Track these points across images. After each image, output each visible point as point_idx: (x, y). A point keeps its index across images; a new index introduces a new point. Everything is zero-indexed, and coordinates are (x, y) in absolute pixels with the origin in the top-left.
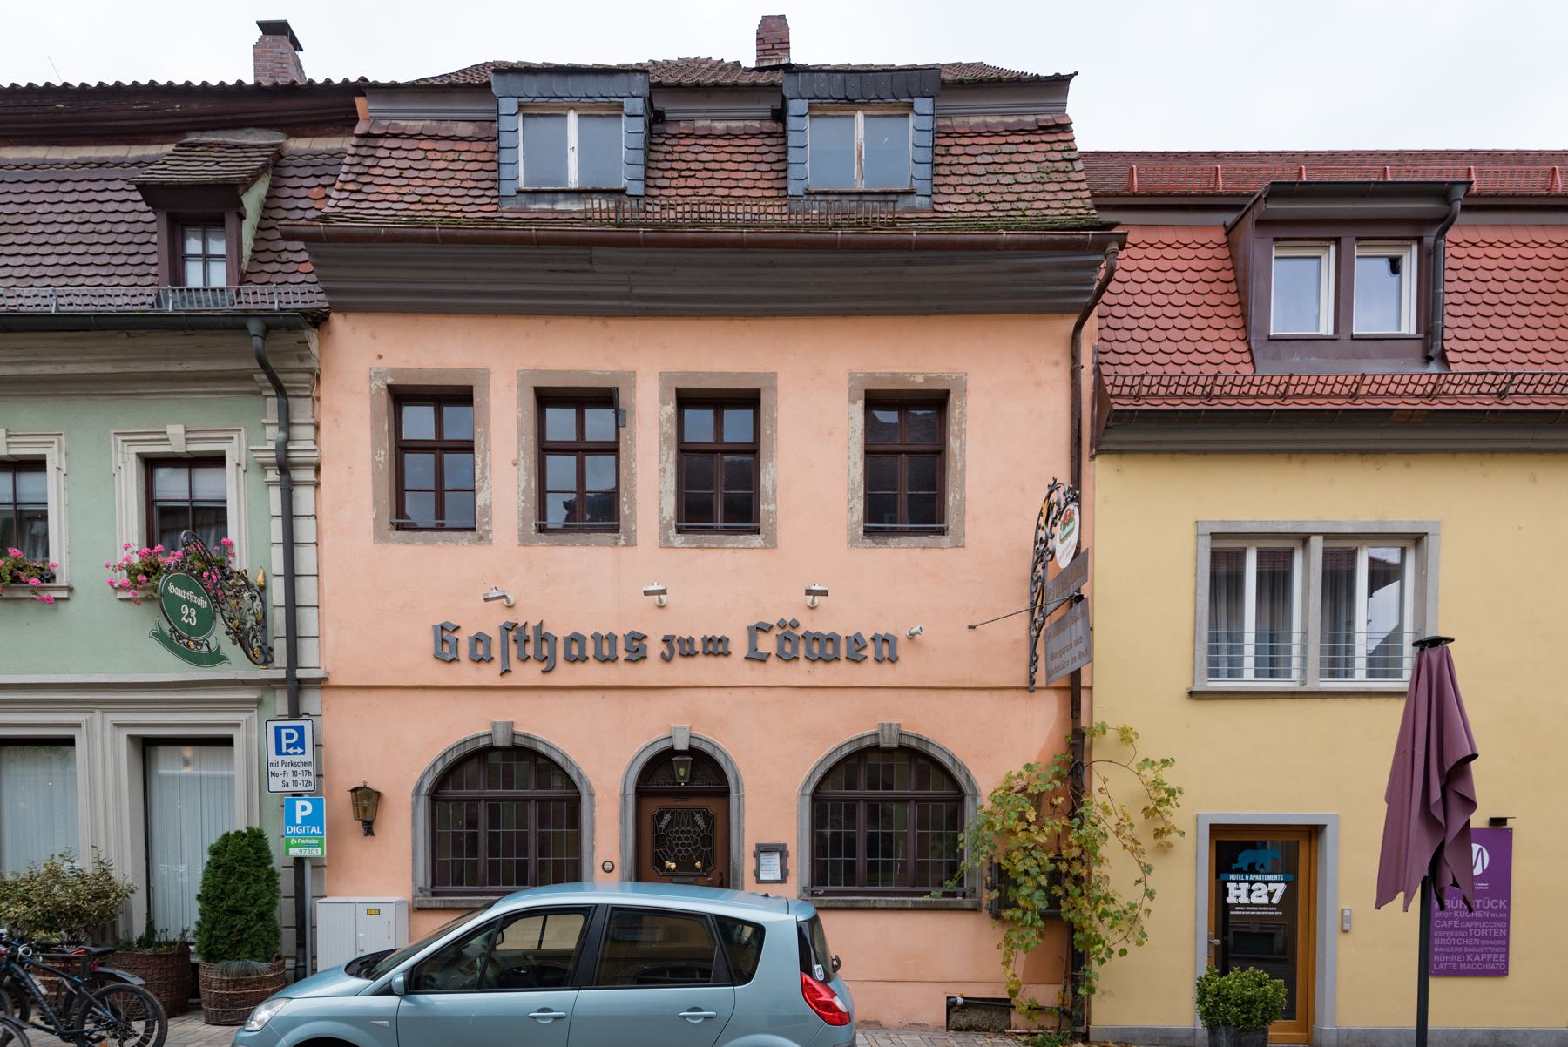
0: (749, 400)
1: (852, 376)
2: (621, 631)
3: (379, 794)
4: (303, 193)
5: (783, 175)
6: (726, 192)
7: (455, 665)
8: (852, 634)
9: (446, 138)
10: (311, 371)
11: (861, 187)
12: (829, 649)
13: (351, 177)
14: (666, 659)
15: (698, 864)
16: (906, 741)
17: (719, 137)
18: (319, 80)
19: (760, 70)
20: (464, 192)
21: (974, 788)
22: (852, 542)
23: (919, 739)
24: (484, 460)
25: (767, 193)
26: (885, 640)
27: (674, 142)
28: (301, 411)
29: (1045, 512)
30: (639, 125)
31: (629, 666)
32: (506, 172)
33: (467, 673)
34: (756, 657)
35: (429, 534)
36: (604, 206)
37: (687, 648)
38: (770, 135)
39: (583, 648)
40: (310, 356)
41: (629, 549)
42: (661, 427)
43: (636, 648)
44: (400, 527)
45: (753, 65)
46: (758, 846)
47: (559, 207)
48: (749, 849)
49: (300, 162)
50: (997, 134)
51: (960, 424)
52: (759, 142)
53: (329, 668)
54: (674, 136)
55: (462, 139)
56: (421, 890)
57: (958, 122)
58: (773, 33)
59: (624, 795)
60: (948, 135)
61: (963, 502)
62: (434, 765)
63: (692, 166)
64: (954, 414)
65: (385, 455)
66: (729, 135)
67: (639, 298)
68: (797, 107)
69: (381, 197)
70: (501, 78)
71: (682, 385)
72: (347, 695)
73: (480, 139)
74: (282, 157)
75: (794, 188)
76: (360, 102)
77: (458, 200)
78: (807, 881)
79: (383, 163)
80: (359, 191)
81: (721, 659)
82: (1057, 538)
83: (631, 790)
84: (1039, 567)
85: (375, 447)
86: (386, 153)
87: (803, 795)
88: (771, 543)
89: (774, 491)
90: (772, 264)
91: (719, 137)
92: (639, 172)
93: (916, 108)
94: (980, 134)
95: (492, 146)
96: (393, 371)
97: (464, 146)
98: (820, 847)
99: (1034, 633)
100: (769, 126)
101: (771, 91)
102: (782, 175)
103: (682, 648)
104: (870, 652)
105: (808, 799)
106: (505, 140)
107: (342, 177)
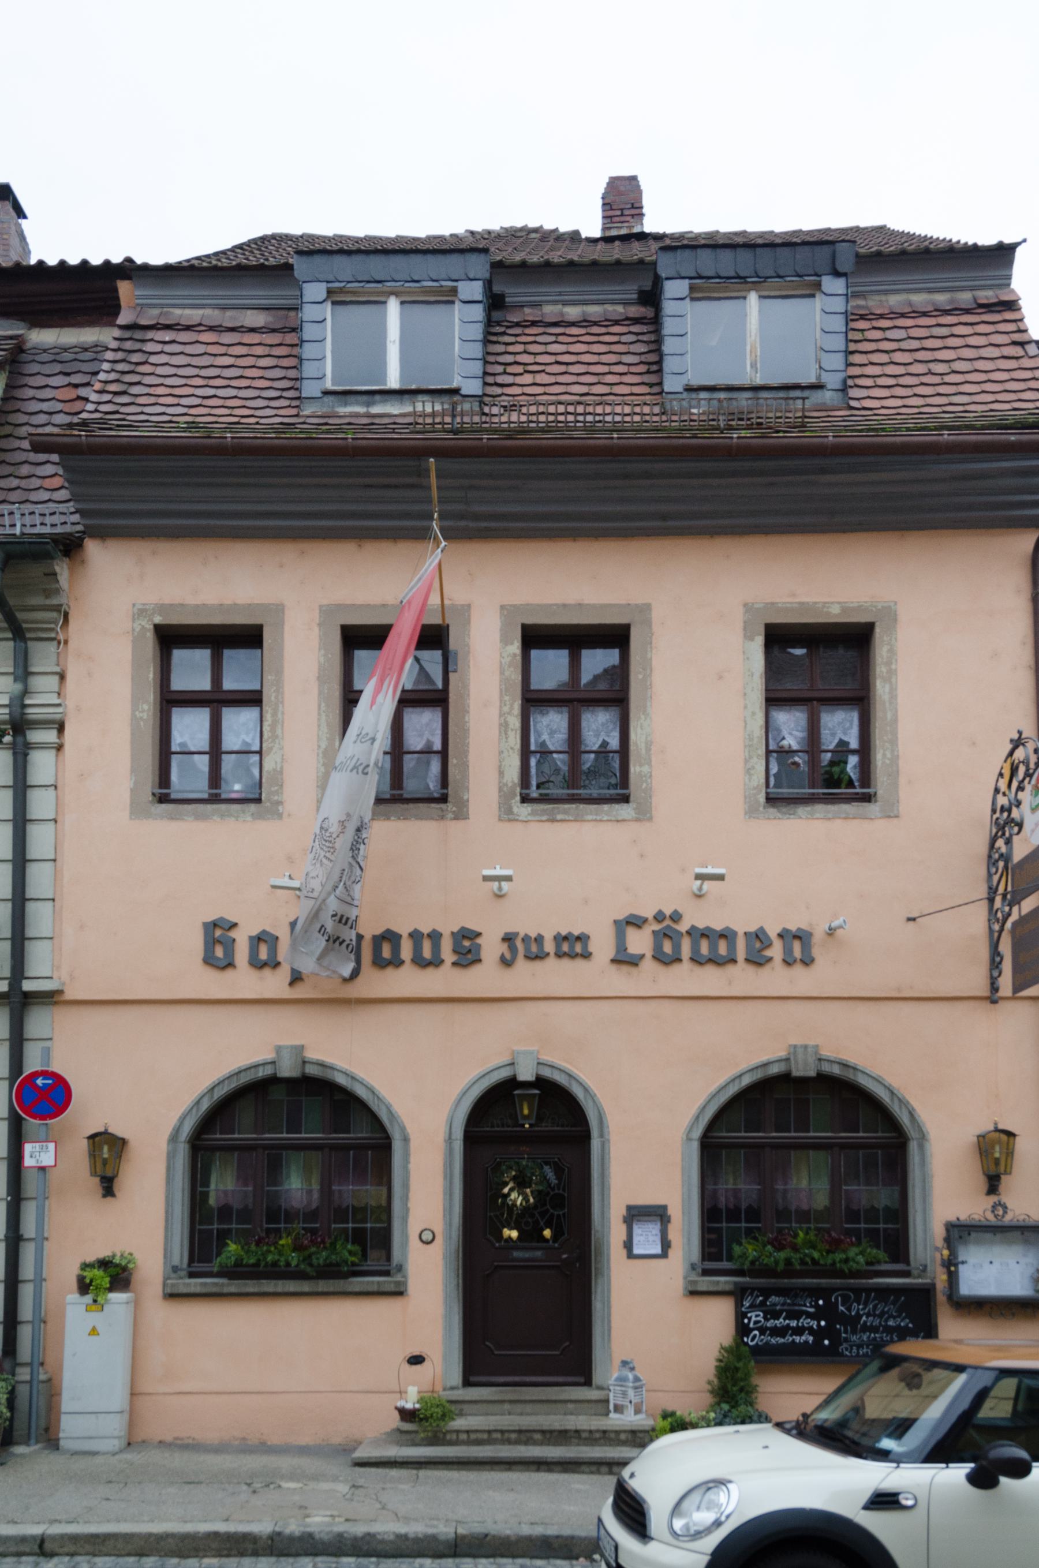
0: (617, 637)
1: (747, 607)
2: (447, 927)
3: (123, 1142)
4: (47, 393)
5: (656, 366)
6: (584, 389)
7: (229, 973)
8: (752, 928)
9: (232, 330)
10: (57, 608)
11: (759, 381)
12: (704, 948)
13: (113, 376)
14: (506, 962)
15: (547, 1233)
16: (826, 1068)
17: (573, 324)
18: (52, 261)
19: (606, 240)
20: (256, 393)
21: (919, 1129)
22: (751, 812)
23: (845, 1065)
24: (275, 714)
25: (636, 390)
26: (796, 937)
27: (517, 331)
28: (43, 657)
29: (1007, 773)
30: (478, 312)
31: (458, 972)
32: (309, 369)
33: (243, 981)
34: (624, 960)
35: (201, 807)
36: (429, 409)
37: (534, 948)
38: (636, 321)
39: (396, 949)
40: (57, 591)
41: (460, 824)
42: (502, 673)
43: (467, 949)
44: (163, 799)
45: (597, 233)
46: (629, 1208)
47: (375, 410)
48: (616, 1212)
49: (45, 357)
50: (925, 314)
51: (889, 663)
52: (624, 329)
53: (65, 977)
54: (517, 325)
55: (252, 330)
56: (175, 1269)
57: (873, 303)
58: (622, 198)
59: (449, 1140)
60: (862, 317)
61: (895, 759)
62: (198, 1103)
63: (540, 359)
64: (881, 651)
65: (148, 709)
66: (585, 322)
67: (476, 517)
68: (674, 289)
69: (152, 400)
70: (304, 259)
71: (531, 620)
72: (86, 1012)
73: (274, 331)
74: (23, 351)
75: (672, 384)
76: (125, 288)
77: (249, 403)
78: (696, 1255)
79: (153, 359)
80: (124, 393)
81: (580, 963)
82: (1025, 807)
83: (459, 1134)
84: (1000, 843)
85: (136, 700)
86: (158, 348)
87: (689, 1139)
88: (644, 815)
89: (648, 749)
90: (647, 475)
91: (573, 324)
92: (477, 368)
93: (824, 288)
94: (903, 315)
95: (291, 338)
96: (161, 608)
97: (255, 338)
98: (712, 1215)
99: (996, 927)
100: (634, 311)
101: (627, 270)
102: (654, 368)
103: (527, 949)
104: (776, 951)
105: (695, 1146)
106: (309, 332)
107: (102, 376)
